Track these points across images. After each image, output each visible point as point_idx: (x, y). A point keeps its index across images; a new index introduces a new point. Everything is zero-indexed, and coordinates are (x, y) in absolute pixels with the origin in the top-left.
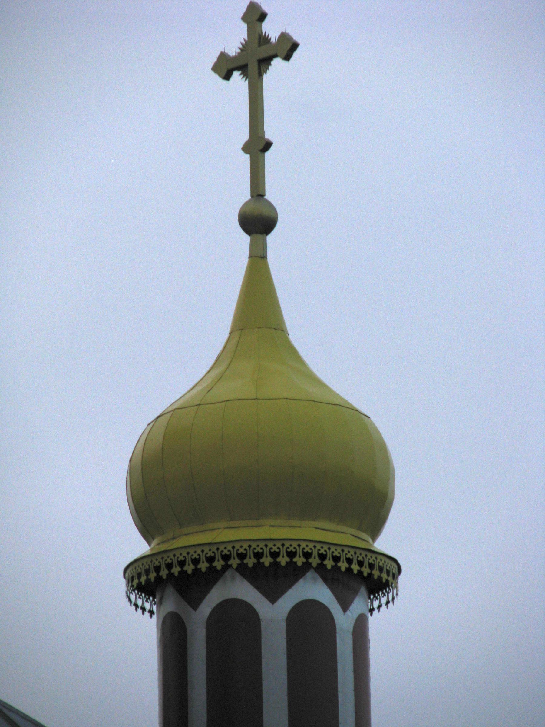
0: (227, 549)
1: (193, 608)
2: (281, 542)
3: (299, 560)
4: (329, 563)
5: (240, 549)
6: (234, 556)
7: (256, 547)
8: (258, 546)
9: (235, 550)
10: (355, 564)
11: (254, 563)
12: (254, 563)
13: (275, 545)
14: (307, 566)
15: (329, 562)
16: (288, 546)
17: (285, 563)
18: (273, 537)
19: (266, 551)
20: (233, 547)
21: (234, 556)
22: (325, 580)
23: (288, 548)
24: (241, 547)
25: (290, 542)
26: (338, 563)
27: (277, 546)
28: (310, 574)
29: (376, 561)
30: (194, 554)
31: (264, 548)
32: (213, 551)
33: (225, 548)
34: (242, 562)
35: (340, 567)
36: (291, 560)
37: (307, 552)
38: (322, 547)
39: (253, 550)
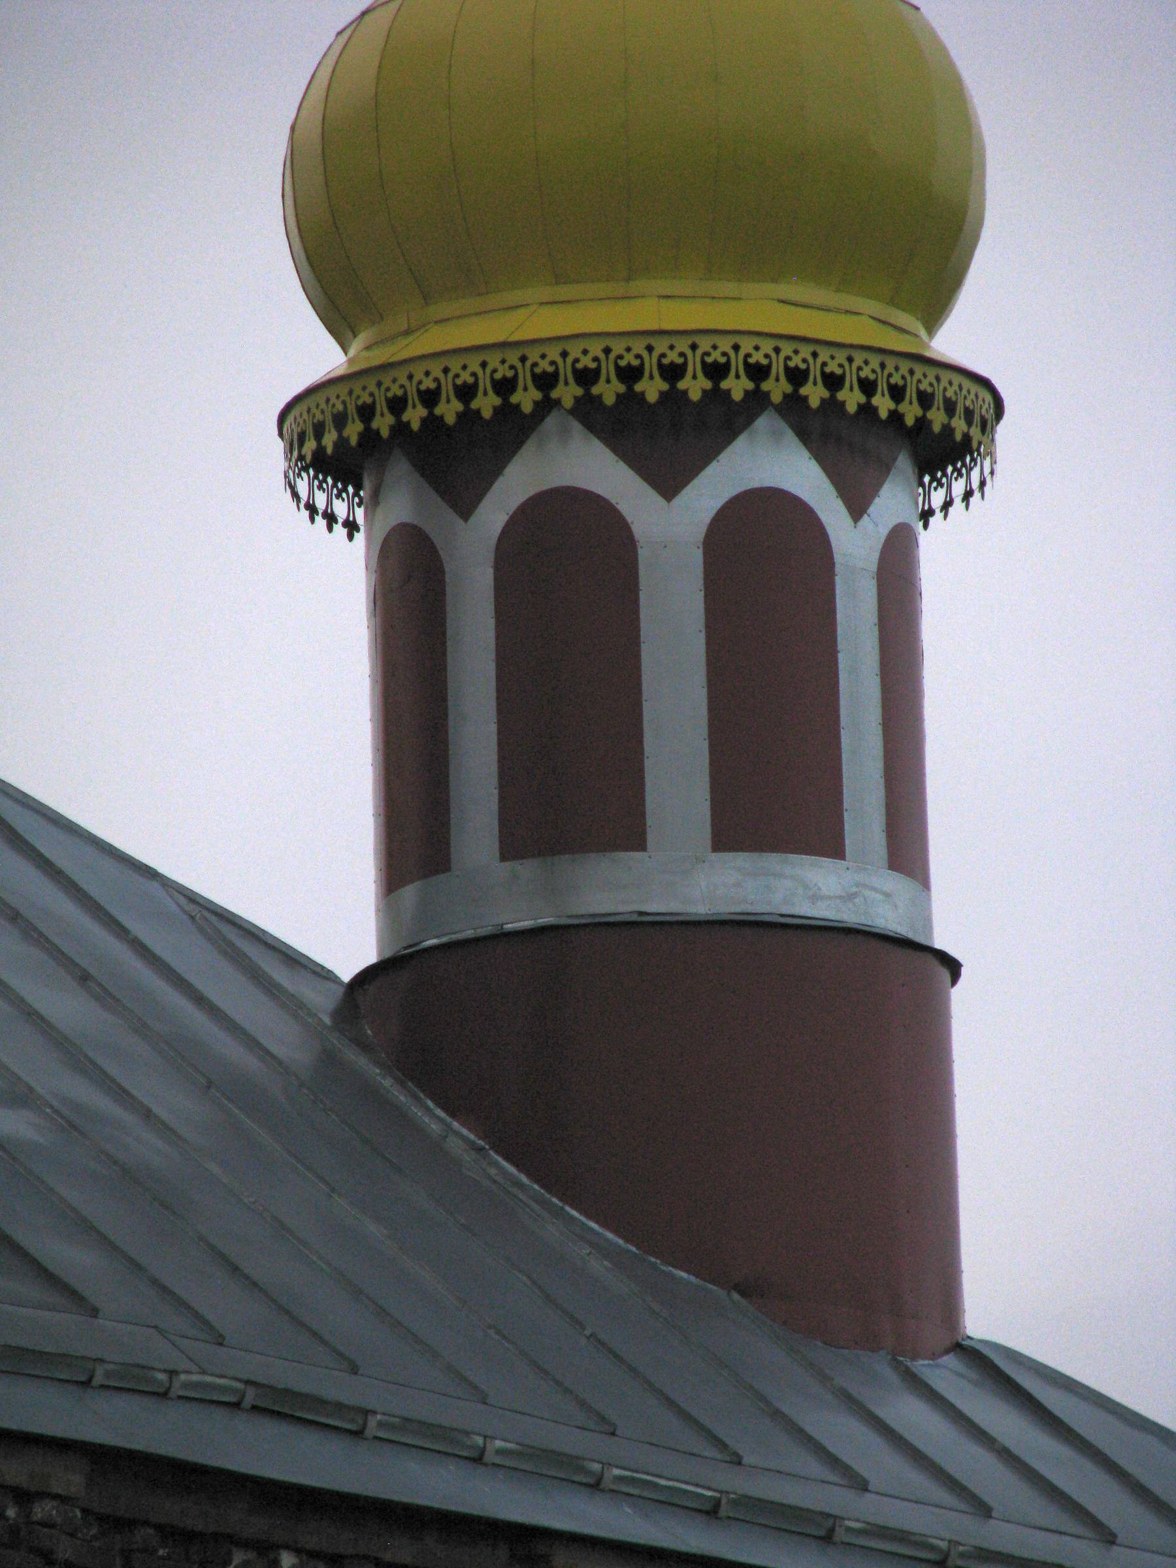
0: (548, 359)
4: (814, 393)
7: (711, 350)
9: (569, 360)
25: (756, 341)
27: (548, 359)
32: (682, 350)
33: (628, 350)
36: (506, 400)
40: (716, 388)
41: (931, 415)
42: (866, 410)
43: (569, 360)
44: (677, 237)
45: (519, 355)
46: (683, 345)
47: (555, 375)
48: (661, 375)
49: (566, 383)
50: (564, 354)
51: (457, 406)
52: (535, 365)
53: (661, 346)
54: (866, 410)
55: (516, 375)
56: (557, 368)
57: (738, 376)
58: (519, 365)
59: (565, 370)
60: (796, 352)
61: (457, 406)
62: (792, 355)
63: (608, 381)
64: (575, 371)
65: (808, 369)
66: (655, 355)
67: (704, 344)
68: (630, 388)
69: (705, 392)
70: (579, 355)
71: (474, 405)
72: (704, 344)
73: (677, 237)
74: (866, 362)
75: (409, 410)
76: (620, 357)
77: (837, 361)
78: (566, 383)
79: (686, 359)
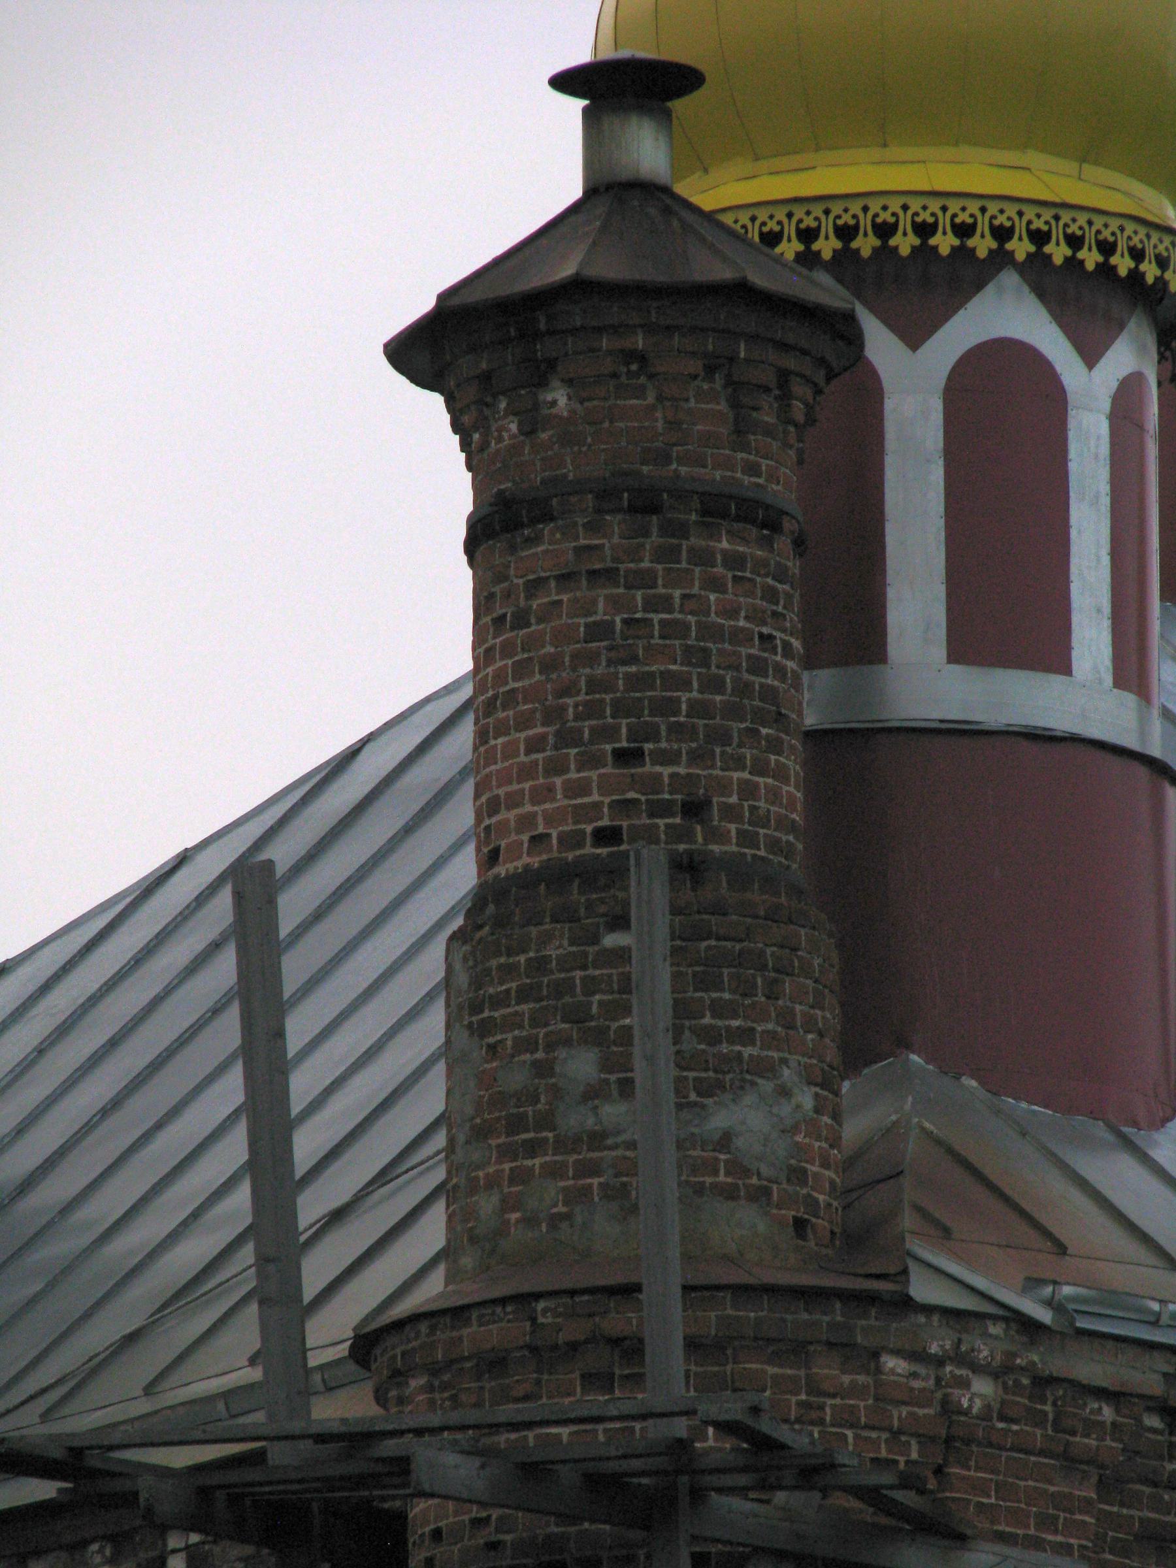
0: (890, 211)
1: (1048, 669)
2: (980, 203)
3: (983, 245)
4: (1058, 252)
5: (960, 213)
6: (789, 234)
7: (998, 214)
8: (925, 208)
9: (870, 214)
10: (1150, 262)
11: (835, 251)
12: (835, 251)
13: (846, 210)
14: (1000, 259)
15: (826, 242)
16: (840, 212)
17: (909, 251)
18: (939, 187)
19: (866, 222)
20: (865, 209)
21: (789, 234)
22: (1041, 293)
23: (839, 217)
24: (885, 208)
25: (962, 202)
26: (813, 242)
27: (851, 213)
28: (1009, 279)
29: (1172, 251)
30: (768, 220)
31: (861, 216)
32: (972, 212)
33: (964, 209)
34: (808, 248)
35: (1115, 268)
36: (924, 243)
37: (1039, 231)
38: (1074, 220)
39: (913, 217)
40: (963, 247)
41: (1143, 267)
42: (1073, 263)
43: (870, 214)
44: (611, 940)
45: (824, 207)
46: (818, 210)
47: (856, 228)
48: (875, 233)
49: (945, 233)
50: (865, 209)
51: (914, 240)
52: (916, 214)
53: (954, 206)
54: (1073, 263)
55: (819, 227)
56: (858, 222)
57: (1020, 239)
58: (785, 221)
59: (866, 222)
60: (1074, 220)
61: (914, 240)
62: (1070, 222)
63: (905, 234)
64: (875, 226)
65: (1083, 236)
66: (949, 214)
67: (875, 206)
68: (808, 248)
69: (953, 248)
70: (840, 212)
71: (815, 247)
72: (875, 206)
73: (611, 940)
74: (1136, 232)
75: (784, 243)
76: (839, 217)
77: (1110, 230)
78: (945, 233)
79: (820, 223)
